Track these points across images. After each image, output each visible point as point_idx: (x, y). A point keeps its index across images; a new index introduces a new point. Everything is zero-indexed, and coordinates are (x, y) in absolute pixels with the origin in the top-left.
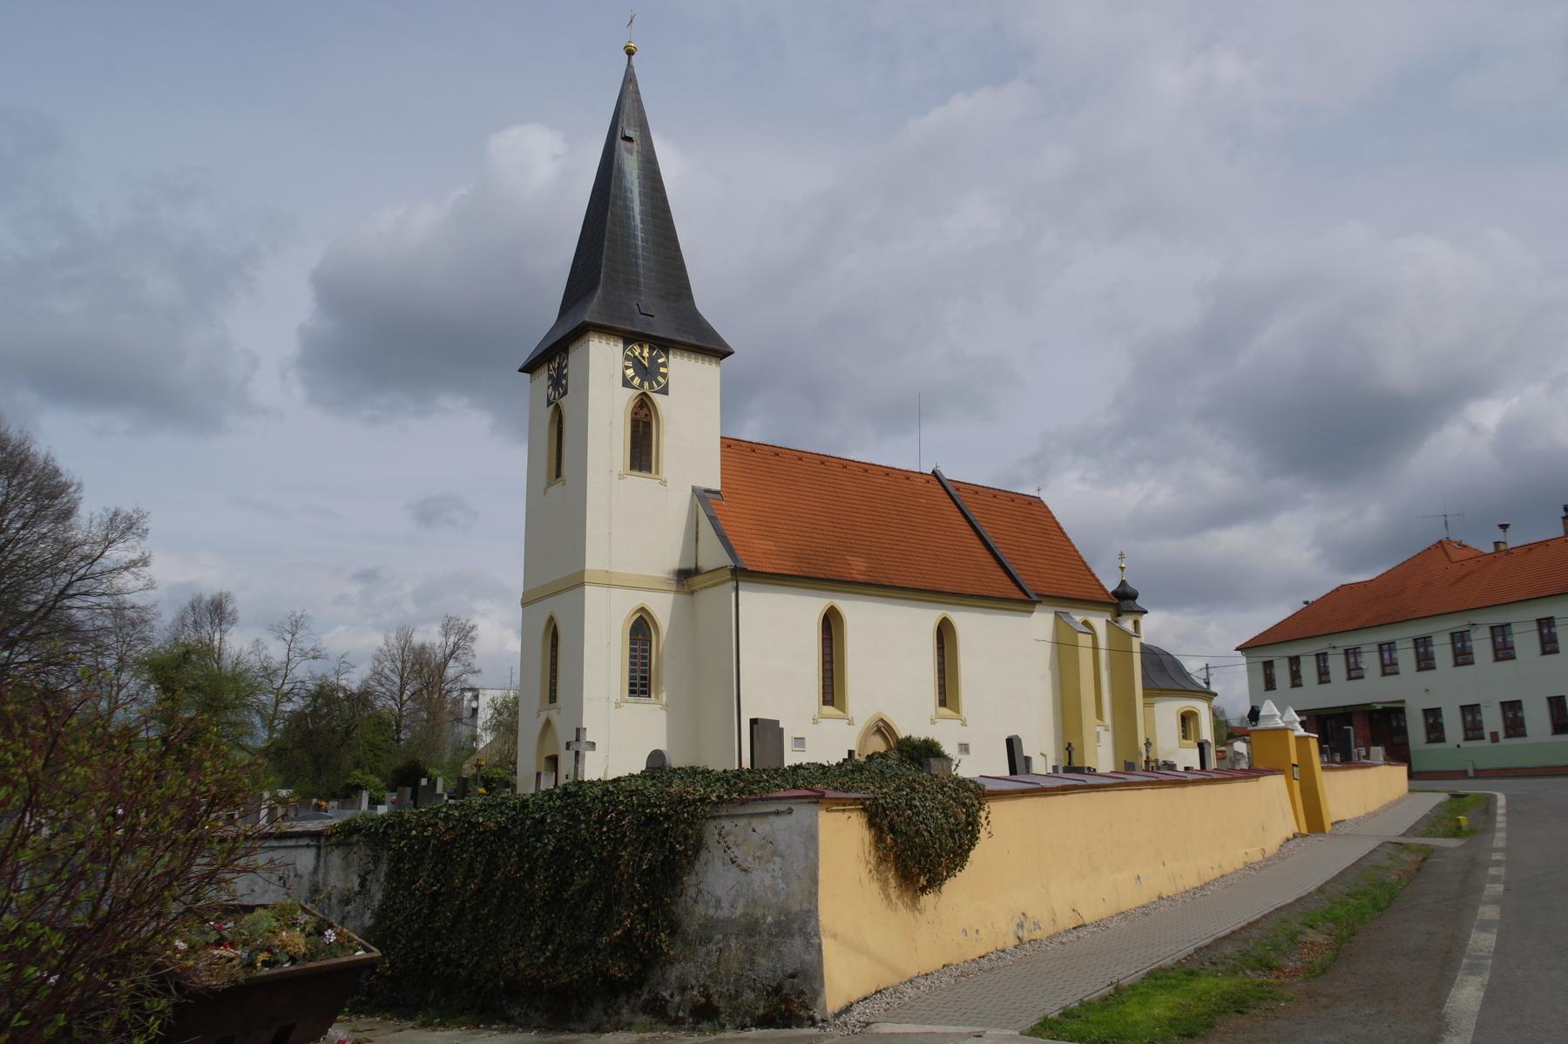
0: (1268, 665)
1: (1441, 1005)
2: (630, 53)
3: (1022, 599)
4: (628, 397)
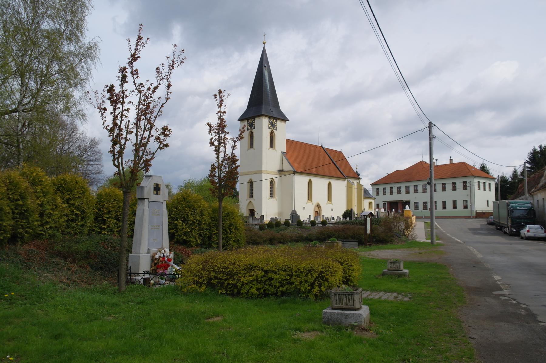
0: (378, 189)
2: (264, 44)
3: (342, 177)
4: (270, 131)
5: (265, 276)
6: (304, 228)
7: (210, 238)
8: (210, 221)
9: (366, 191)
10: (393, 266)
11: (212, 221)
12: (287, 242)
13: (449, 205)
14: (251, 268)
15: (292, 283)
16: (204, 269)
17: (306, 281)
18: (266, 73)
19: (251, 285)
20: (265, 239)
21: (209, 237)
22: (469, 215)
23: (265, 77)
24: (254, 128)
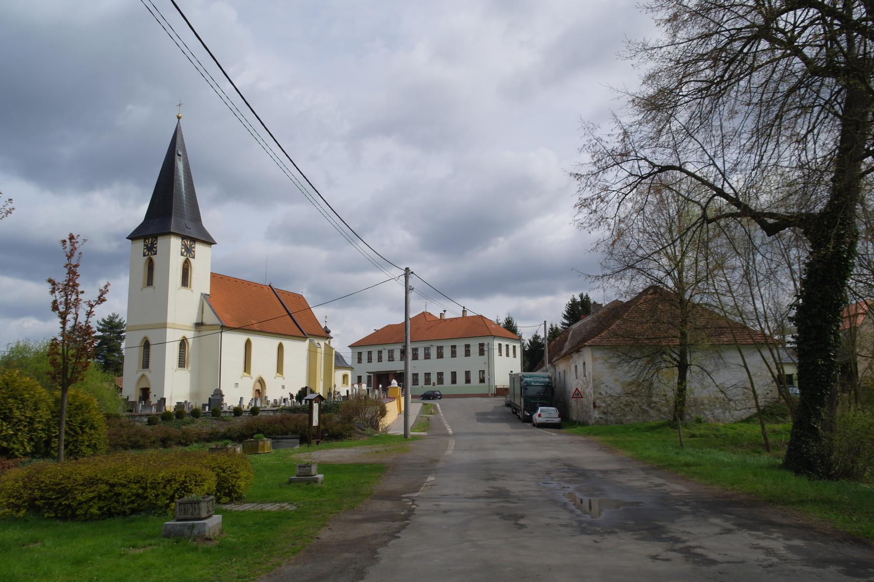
0: (360, 354)
1: (843, 134)
2: (179, 118)
3: (301, 335)
4: (183, 258)
5: (110, 491)
6: (223, 419)
7: (48, 443)
8: (50, 417)
9: (338, 357)
10: (302, 470)
11: (53, 417)
12: (191, 442)
13: (461, 378)
14: (91, 482)
15: (147, 498)
16: (25, 487)
17: (164, 494)
18: (180, 165)
19: (91, 503)
20: (153, 439)
21: (45, 442)
22: (485, 392)
23: (177, 172)
24: (155, 254)
